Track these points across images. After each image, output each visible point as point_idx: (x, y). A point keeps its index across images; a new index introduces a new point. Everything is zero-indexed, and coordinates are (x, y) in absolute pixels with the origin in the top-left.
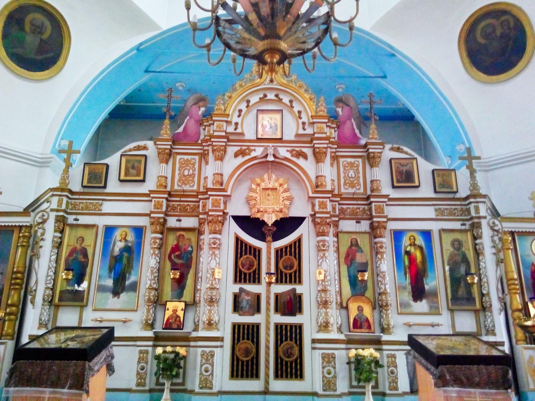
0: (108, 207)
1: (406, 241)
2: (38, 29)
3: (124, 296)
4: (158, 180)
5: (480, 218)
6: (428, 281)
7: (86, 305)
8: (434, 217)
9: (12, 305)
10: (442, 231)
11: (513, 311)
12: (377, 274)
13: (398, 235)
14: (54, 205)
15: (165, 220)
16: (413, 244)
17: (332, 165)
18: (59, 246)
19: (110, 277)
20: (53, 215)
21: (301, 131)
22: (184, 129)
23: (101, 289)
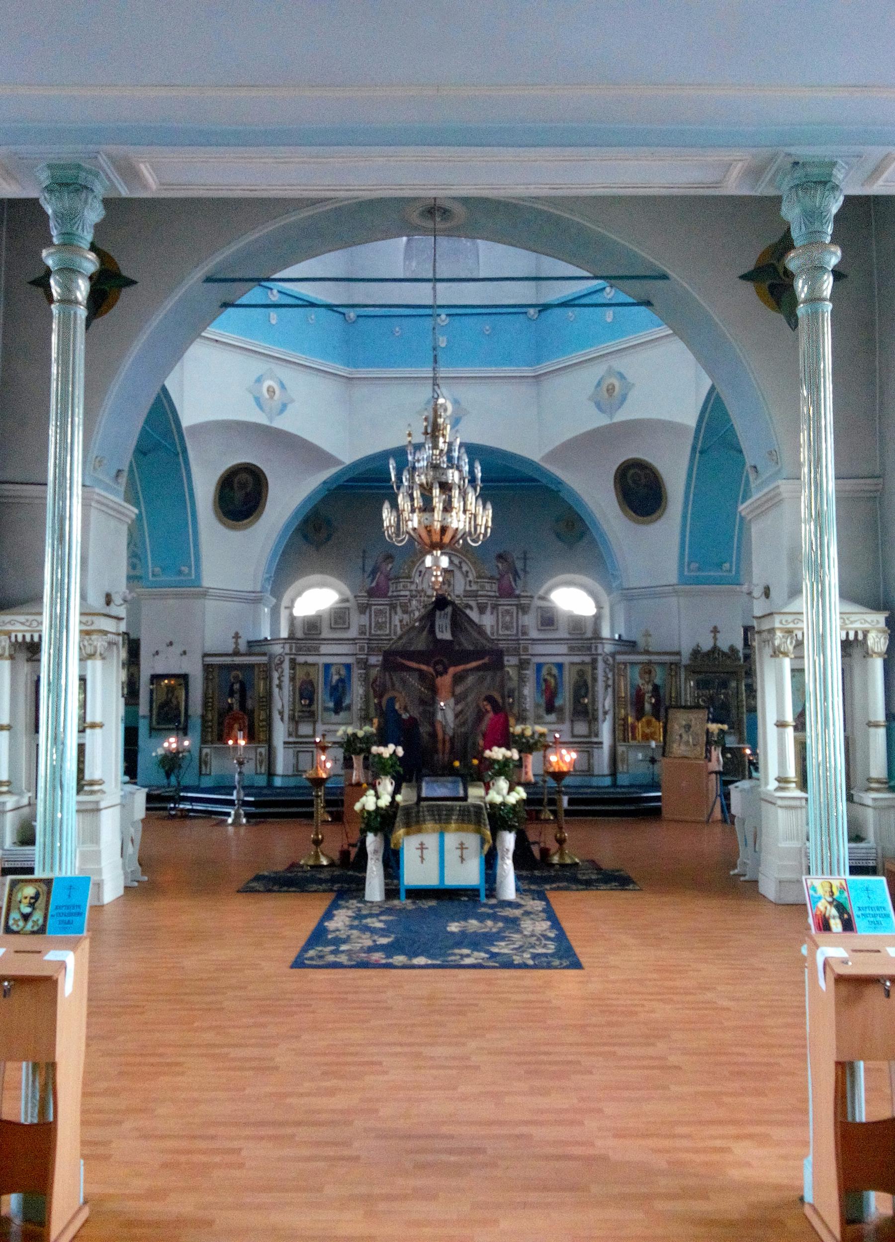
0: (324, 649)
1: (544, 671)
2: (243, 486)
3: (342, 714)
5: (598, 655)
9: (262, 721)
10: (572, 664)
12: (522, 696)
13: (539, 666)
14: (287, 650)
15: (367, 659)
16: (550, 674)
17: (492, 613)
18: (293, 679)
20: (287, 658)
21: (468, 588)
23: (326, 709)
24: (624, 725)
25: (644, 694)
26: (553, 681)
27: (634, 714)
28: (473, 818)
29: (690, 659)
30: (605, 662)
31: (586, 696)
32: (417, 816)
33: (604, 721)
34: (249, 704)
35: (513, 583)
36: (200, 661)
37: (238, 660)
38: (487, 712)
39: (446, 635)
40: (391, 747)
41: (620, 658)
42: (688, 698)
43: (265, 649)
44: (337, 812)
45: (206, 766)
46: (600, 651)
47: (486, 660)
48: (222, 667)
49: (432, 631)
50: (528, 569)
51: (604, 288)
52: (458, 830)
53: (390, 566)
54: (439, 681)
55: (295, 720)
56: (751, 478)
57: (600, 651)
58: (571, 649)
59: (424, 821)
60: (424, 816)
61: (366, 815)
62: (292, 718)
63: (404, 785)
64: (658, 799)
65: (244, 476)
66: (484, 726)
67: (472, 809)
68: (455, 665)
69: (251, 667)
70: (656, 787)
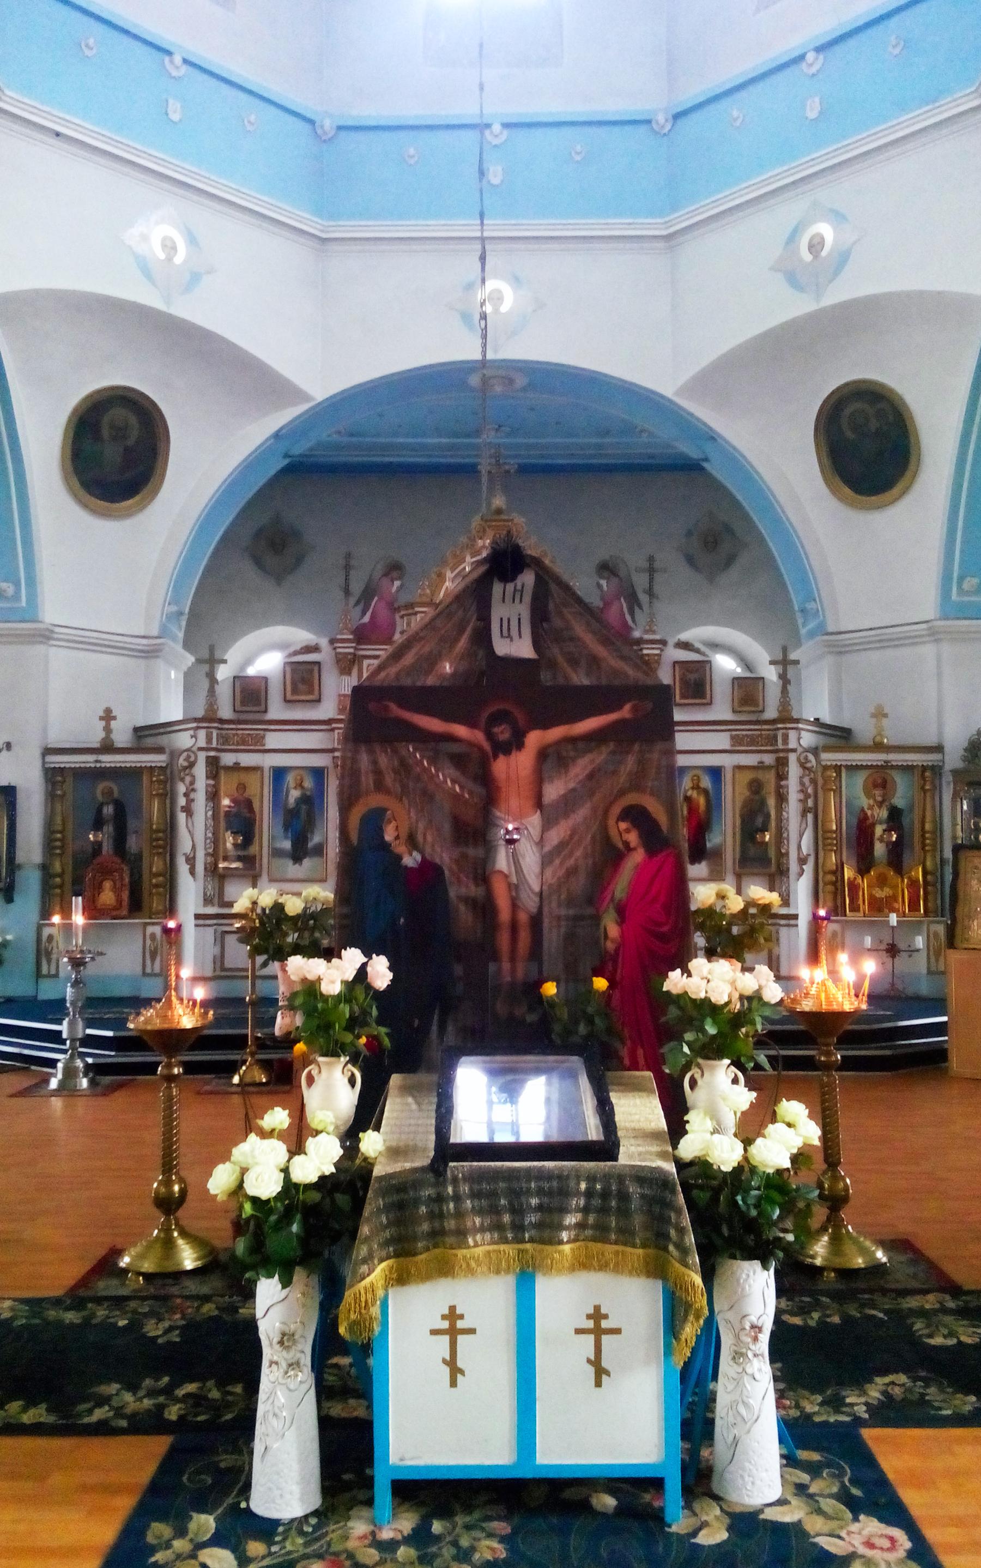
0: (273, 740)
2: (120, 432)
3: (307, 862)
4: (340, 701)
6: (712, 836)
7: (260, 875)
8: (728, 747)
9: (157, 875)
10: (739, 768)
11: (825, 873)
14: (202, 743)
16: (696, 787)
18: (213, 796)
19: (286, 838)
20: (202, 756)
22: (372, 617)
23: (277, 853)
24: (834, 884)
25: (873, 825)
26: (702, 801)
27: (854, 862)
28: (638, 1220)
29: (965, 759)
30: (803, 765)
31: (764, 829)
32: (437, 1216)
33: (801, 873)
34: (133, 843)
35: (628, 618)
36: (38, 763)
37: (109, 760)
38: (628, 848)
39: (523, 648)
40: (352, 958)
41: (829, 758)
42: (959, 834)
43: (163, 740)
44: (281, 1061)
45: (49, 961)
46: (792, 744)
47: (625, 712)
48: (81, 774)
49: (483, 637)
50: (657, 588)
51: (802, 57)
52: (582, 1264)
53: (397, 583)
54: (500, 766)
55: (217, 876)
56: (800, 621)
57: (792, 744)
58: (736, 740)
59: (461, 1233)
60: (459, 1214)
61: (248, 1209)
62: (212, 870)
63: (395, 1080)
64: (939, 1029)
65: (119, 414)
66: (621, 886)
67: (633, 1189)
68: (545, 726)
69: (135, 773)
70: (937, 1004)
